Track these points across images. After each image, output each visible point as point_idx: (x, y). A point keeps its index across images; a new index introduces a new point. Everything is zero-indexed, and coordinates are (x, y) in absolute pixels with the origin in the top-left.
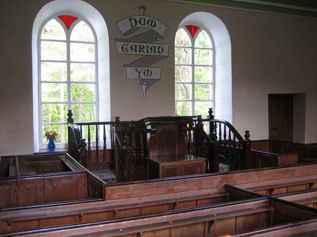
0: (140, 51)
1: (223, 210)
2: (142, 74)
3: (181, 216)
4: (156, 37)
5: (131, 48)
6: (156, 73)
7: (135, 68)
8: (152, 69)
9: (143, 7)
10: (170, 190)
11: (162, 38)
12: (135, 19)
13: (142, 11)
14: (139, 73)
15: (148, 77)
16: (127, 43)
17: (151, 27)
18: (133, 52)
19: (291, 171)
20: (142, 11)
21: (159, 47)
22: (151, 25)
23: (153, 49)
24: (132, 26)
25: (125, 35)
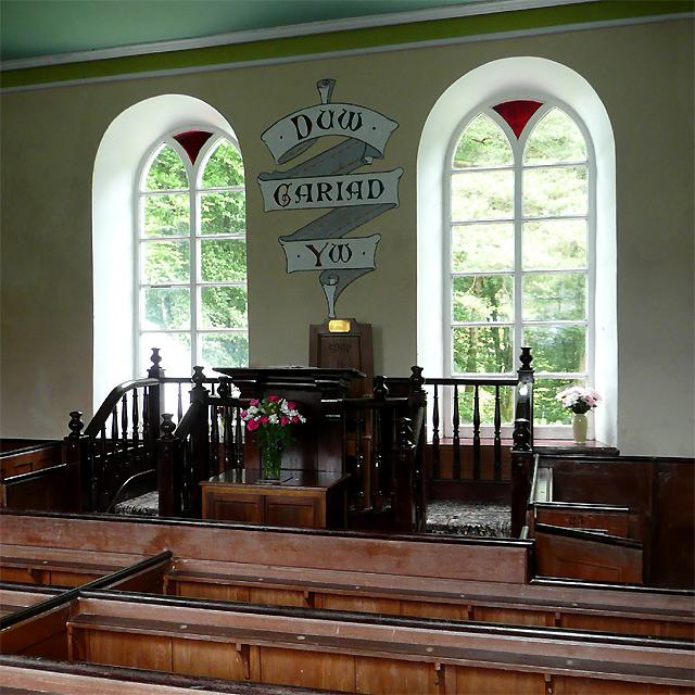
0: (320, 199)
1: (206, 620)
2: (325, 258)
3: (337, 629)
4: (364, 153)
5: (298, 193)
6: (362, 252)
7: (308, 243)
8: (352, 243)
9: (326, 82)
10: (30, 539)
11: (379, 155)
12: (305, 117)
13: (324, 92)
14: (318, 255)
15: (341, 265)
16: (287, 182)
17: (348, 132)
18: (303, 203)
19: (392, 551)
20: (324, 92)
21: (371, 182)
22: (350, 124)
23: (355, 188)
24: (300, 137)
25: (283, 161)
